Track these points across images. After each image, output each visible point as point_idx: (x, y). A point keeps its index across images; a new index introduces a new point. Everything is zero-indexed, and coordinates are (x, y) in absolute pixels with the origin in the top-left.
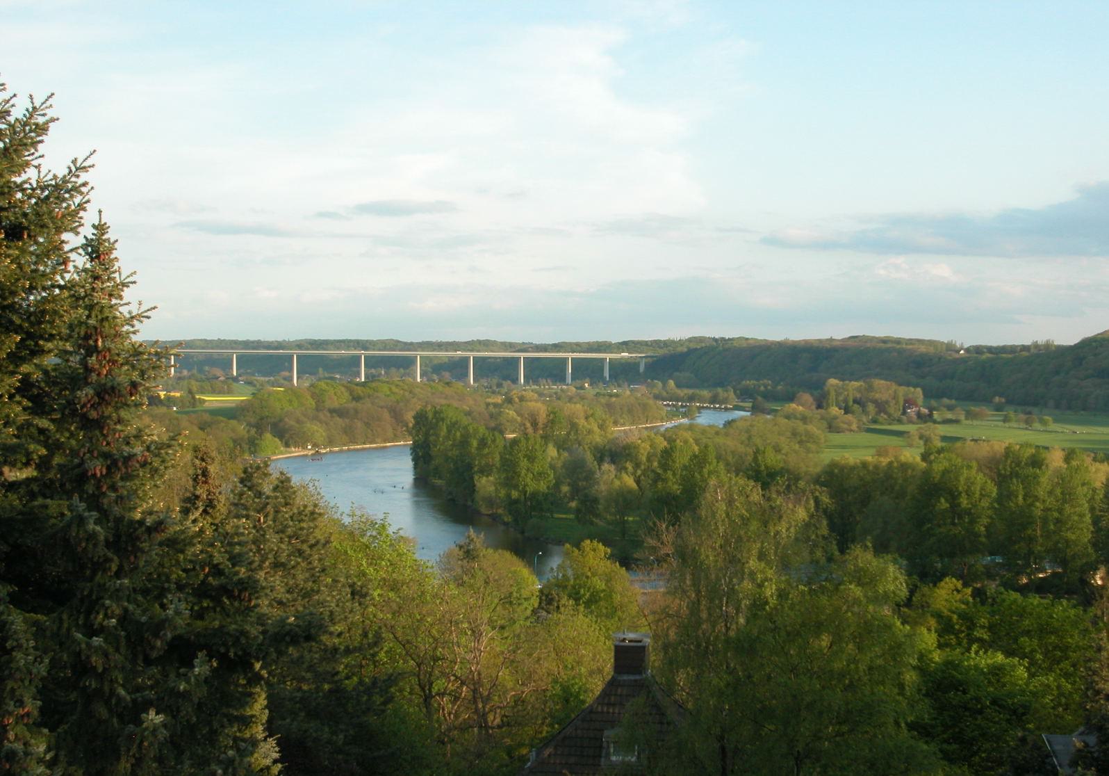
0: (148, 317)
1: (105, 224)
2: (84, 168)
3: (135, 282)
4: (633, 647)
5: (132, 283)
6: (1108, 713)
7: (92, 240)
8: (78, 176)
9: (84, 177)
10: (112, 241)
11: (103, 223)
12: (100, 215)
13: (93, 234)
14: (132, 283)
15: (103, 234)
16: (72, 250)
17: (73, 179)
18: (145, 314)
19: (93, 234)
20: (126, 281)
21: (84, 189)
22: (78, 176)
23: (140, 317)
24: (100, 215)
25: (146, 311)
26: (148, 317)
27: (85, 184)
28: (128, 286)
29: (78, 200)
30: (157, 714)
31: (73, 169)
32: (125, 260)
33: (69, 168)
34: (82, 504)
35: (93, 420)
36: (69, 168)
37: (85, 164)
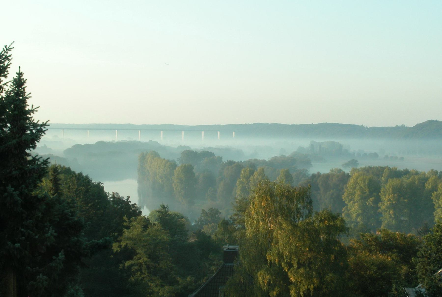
0: (37, 111)
1: (22, 72)
2: (10, 49)
3: (31, 97)
4: (228, 251)
5: (29, 97)
6: (441, 287)
7: (16, 79)
8: (7, 53)
9: (9, 53)
10: (24, 80)
11: (21, 72)
12: (20, 69)
13: (17, 77)
14: (29, 97)
15: (21, 77)
16: (4, 85)
17: (5, 54)
18: (35, 110)
19: (17, 77)
20: (27, 96)
21: (10, 58)
22: (7, 53)
23: (32, 111)
24: (20, 69)
25: (35, 109)
26: (37, 111)
27: (10, 56)
28: (28, 99)
29: (6, 63)
30: (43, 275)
31: (5, 50)
32: (29, 88)
33: (4, 49)
34: (12, 188)
35: (111, 255)
36: (4, 49)
37: (11, 47)
